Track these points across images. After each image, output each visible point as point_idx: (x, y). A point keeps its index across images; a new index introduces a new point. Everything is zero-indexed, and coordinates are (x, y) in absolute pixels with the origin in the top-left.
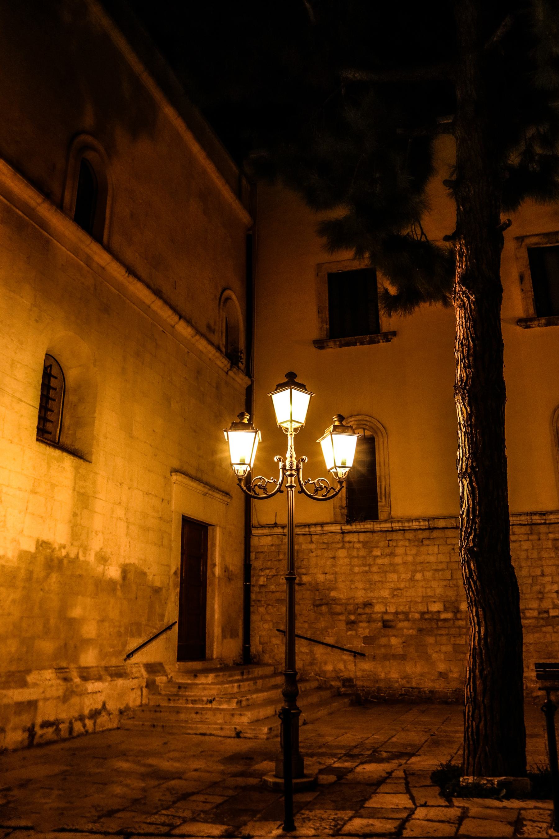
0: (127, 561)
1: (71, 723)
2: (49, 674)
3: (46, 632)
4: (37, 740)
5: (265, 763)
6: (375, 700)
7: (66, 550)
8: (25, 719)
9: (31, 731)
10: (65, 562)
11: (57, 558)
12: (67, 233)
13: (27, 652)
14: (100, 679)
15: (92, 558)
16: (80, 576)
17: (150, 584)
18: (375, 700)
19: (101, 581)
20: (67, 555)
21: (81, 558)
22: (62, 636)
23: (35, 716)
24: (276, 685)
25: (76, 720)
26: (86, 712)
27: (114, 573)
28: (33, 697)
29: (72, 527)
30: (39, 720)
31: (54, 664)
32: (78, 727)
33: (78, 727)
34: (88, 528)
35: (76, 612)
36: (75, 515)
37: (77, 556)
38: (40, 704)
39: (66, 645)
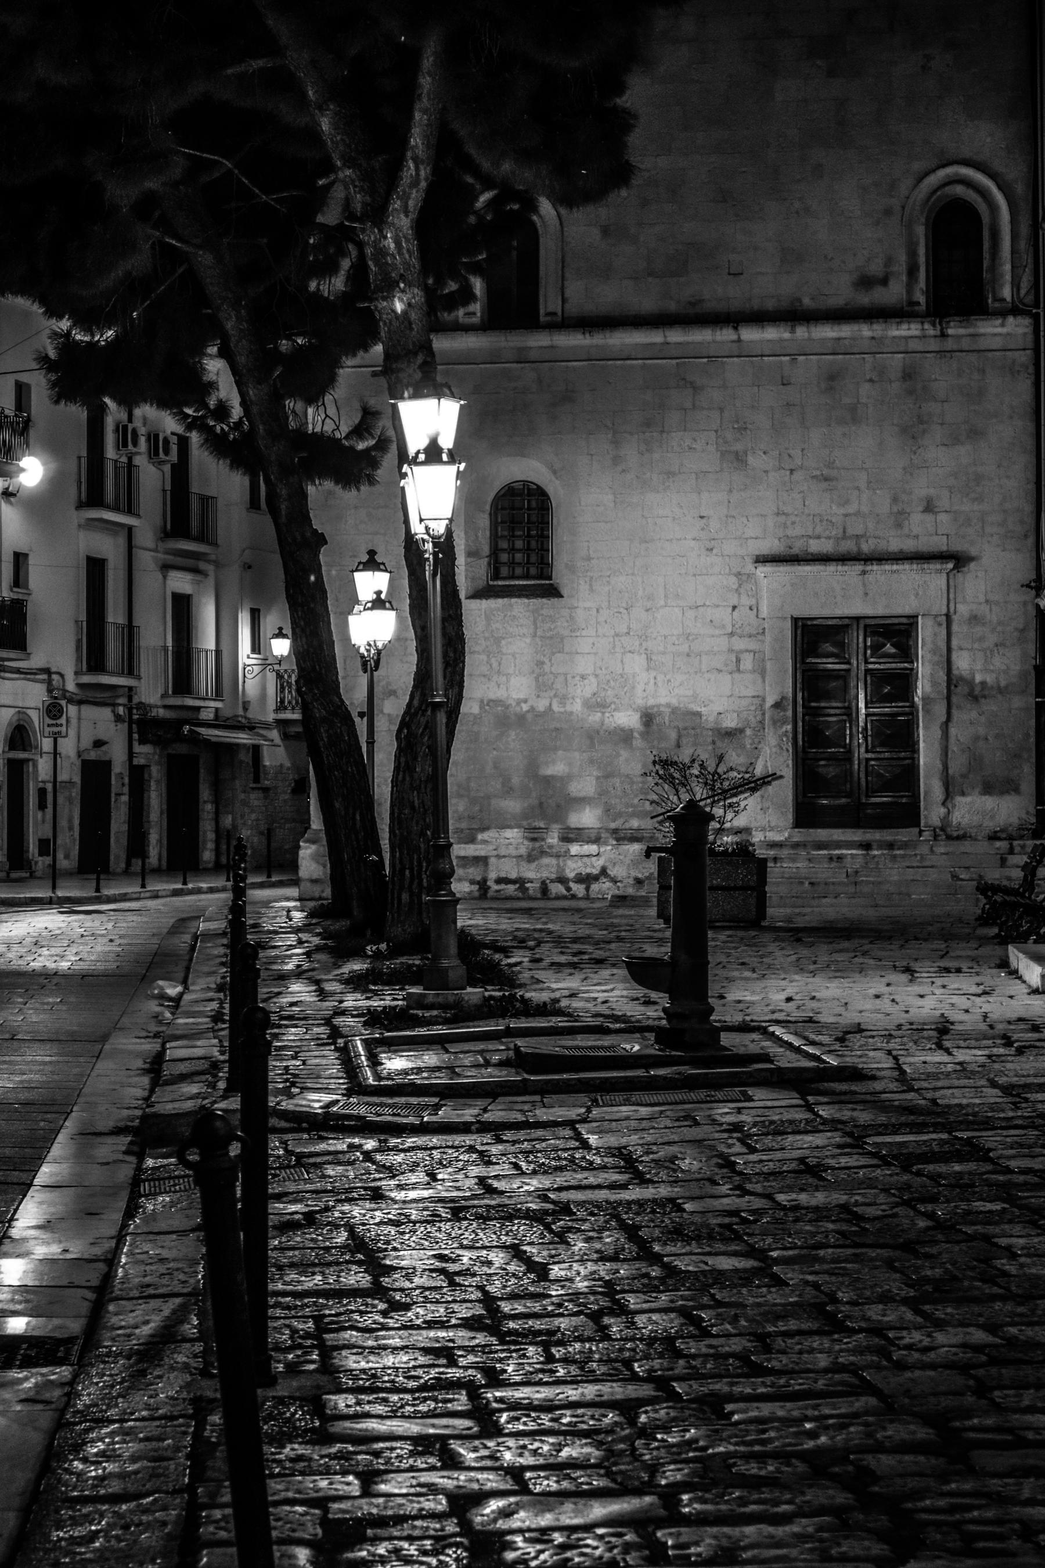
0: (651, 702)
1: (543, 883)
2: (513, 835)
3: (508, 790)
4: (490, 894)
5: (726, 1267)
6: (358, 817)
7: (530, 703)
8: (475, 873)
9: (483, 885)
10: (529, 716)
11: (516, 714)
12: (471, 345)
13: (481, 811)
14: (597, 840)
15: (576, 707)
16: (557, 729)
17: (711, 725)
18: (358, 817)
19: (598, 732)
20: (532, 709)
21: (556, 707)
22: (534, 794)
23: (486, 871)
24: (754, 790)
25: (552, 881)
26: (571, 875)
27: (627, 719)
28: (483, 853)
29: (537, 679)
30: (492, 875)
31: (525, 823)
32: (557, 889)
33: (557, 889)
34: (566, 674)
35: (557, 768)
36: (540, 664)
37: (550, 707)
38: (492, 861)
39: (541, 804)
